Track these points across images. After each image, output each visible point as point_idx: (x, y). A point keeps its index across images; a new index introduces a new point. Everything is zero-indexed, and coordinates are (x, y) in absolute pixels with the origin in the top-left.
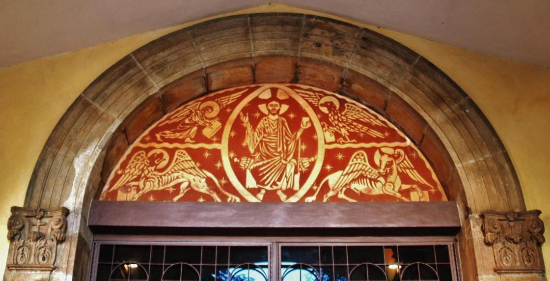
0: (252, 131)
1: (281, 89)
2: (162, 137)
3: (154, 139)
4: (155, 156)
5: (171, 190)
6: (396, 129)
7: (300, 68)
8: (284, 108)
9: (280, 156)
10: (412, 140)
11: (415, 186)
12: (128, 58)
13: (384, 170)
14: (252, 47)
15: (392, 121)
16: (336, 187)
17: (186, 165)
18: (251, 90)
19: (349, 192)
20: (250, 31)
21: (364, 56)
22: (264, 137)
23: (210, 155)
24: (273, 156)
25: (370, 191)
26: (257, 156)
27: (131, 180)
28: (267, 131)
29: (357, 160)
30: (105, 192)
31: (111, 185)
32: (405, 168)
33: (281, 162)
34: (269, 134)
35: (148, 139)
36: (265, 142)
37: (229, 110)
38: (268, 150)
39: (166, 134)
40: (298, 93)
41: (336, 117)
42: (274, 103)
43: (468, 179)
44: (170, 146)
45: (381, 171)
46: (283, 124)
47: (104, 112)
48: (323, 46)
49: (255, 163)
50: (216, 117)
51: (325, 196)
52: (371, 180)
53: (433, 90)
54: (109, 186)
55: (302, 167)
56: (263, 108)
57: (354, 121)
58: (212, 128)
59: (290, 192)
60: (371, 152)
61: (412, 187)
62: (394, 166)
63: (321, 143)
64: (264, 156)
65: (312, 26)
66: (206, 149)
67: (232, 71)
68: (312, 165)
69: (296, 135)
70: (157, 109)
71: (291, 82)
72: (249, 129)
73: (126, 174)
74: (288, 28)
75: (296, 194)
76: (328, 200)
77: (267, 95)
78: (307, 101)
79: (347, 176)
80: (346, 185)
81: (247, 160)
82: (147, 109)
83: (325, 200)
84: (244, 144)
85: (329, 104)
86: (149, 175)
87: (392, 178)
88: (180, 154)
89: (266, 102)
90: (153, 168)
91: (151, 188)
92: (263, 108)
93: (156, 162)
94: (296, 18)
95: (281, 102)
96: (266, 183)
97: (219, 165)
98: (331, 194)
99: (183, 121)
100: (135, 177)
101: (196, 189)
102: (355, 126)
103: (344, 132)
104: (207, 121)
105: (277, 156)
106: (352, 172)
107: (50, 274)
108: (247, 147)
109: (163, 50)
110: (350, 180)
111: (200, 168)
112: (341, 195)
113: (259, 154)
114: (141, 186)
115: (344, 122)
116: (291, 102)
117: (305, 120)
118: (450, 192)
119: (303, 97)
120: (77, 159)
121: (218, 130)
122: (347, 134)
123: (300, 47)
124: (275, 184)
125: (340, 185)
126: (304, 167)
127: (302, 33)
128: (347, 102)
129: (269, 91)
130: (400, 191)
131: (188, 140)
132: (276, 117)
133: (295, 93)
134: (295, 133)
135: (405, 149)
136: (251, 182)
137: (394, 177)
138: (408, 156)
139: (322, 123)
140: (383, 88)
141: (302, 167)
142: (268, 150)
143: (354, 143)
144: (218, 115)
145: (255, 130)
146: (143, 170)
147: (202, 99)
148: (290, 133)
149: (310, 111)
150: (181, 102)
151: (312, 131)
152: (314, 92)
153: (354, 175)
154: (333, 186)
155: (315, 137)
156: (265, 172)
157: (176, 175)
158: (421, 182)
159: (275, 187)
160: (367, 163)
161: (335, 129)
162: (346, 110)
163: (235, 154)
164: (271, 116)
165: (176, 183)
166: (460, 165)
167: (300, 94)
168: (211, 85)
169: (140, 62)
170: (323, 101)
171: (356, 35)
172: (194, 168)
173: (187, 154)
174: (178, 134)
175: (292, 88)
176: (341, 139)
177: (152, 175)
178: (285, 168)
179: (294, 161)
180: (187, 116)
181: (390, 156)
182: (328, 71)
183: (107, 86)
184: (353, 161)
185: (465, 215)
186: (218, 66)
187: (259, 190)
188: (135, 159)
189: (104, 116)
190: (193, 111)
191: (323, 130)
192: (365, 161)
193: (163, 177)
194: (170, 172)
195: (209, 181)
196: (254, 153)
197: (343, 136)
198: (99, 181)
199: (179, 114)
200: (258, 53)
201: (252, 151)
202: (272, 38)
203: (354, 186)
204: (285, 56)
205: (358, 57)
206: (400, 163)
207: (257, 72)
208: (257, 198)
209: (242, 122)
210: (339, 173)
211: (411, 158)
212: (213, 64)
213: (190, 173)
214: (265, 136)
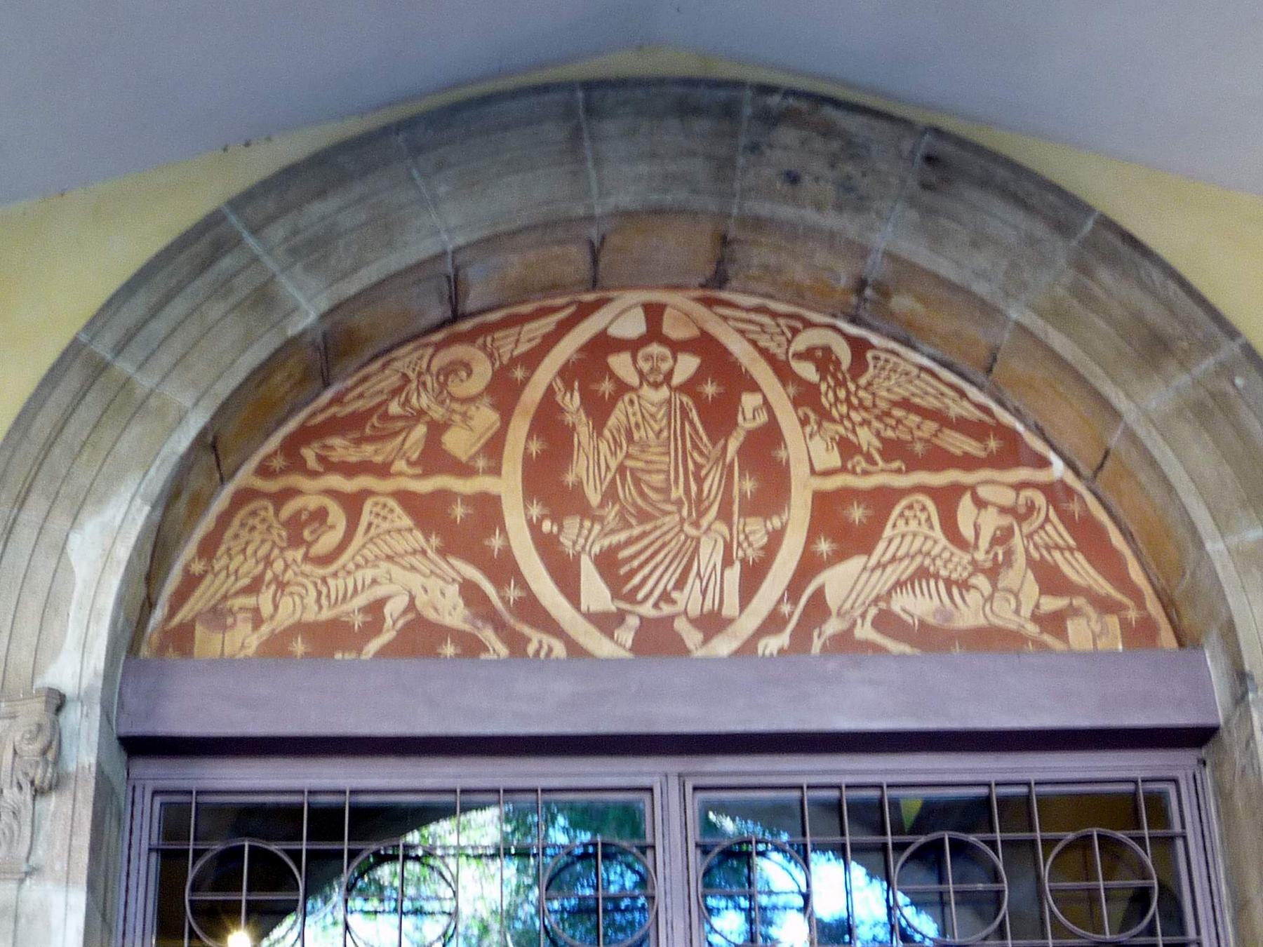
0: (591, 437)
1: (674, 307)
2: (321, 459)
3: (297, 465)
4: (304, 517)
5: (358, 620)
6: (1020, 427)
7: (735, 247)
8: (687, 365)
9: (680, 511)
10: (1070, 464)
11: (1079, 601)
12: (213, 220)
13: (987, 552)
14: (594, 185)
15: (1009, 404)
16: (847, 606)
17: (400, 544)
18: (585, 311)
19: (887, 622)
20: (586, 135)
21: (928, 212)
22: (628, 456)
23: (470, 512)
24: (657, 514)
25: (948, 617)
26: (611, 513)
27: (233, 591)
28: (636, 436)
29: (907, 523)
30: (154, 629)
31: (173, 612)
32: (1048, 548)
33: (682, 530)
34: (644, 447)
35: (278, 463)
36: (633, 471)
37: (519, 373)
38: (642, 494)
39: (332, 448)
40: (725, 318)
41: (842, 394)
42: (655, 349)
43: (1243, 587)
44: (349, 485)
45: (980, 556)
46: (685, 413)
47: (152, 391)
48: (807, 180)
49: (606, 535)
50: (480, 395)
51: (816, 633)
52: (949, 583)
53: (1139, 317)
54: (166, 610)
55: (745, 545)
56: (620, 363)
57: (895, 404)
58: (471, 429)
59: (712, 623)
60: (946, 499)
61: (1071, 604)
62: (1017, 542)
63: (799, 472)
64: (631, 514)
65: (771, 120)
66: (456, 494)
67: (531, 256)
68: (776, 538)
69: (725, 449)
70: (305, 379)
71: (703, 286)
72: (584, 432)
73: (216, 575)
74: (702, 125)
75: (730, 629)
76: (824, 645)
77: (632, 326)
78: (754, 343)
79: (878, 572)
80: (876, 600)
81: (581, 526)
82: (278, 378)
83: (817, 645)
84: (570, 479)
85: (819, 354)
86: (289, 575)
87: (1009, 578)
88: (378, 509)
89: (633, 346)
90: (299, 554)
91: (297, 616)
92: (620, 363)
93: (306, 534)
94: (722, 94)
95: (677, 347)
96: (640, 596)
97: (496, 542)
98: (833, 626)
99: (383, 408)
100: (245, 581)
101: (431, 615)
102: (899, 421)
103: (865, 437)
104: (456, 406)
105: (669, 513)
106: (893, 559)
107: (19, 889)
108: (579, 486)
109: (321, 194)
110: (889, 584)
111: (443, 552)
112: (865, 632)
113: (617, 507)
114: (266, 609)
115: (866, 409)
116: (705, 345)
117: (749, 401)
118: (1186, 622)
119: (742, 332)
120: (78, 536)
121: (489, 434)
122: (877, 443)
123: (737, 185)
124: (666, 597)
125: (860, 601)
126: (750, 545)
127: (743, 141)
128: (872, 347)
129: (639, 315)
130: (1036, 618)
131: (400, 465)
132: (664, 392)
133: (717, 318)
134: (722, 442)
135: (1048, 489)
136: (595, 593)
137: (1019, 576)
138: (1056, 509)
139: (801, 412)
140: (987, 311)
141: (745, 545)
142: (642, 494)
143: (899, 471)
144: (490, 389)
145: (600, 434)
146: (268, 562)
147: (438, 337)
148: (705, 438)
149: (762, 372)
150: (376, 350)
151: (770, 435)
152: (774, 315)
153: (898, 572)
154: (839, 603)
155: (782, 454)
156: (636, 563)
157: (369, 573)
158: (1095, 587)
159: (667, 609)
160: (938, 533)
161: (841, 430)
162: (871, 371)
163: (544, 506)
164: (646, 391)
165: (372, 598)
166: (1220, 546)
167: (731, 323)
168: (466, 294)
169: (255, 231)
170: (800, 344)
171: (906, 145)
172: (424, 552)
173: (398, 510)
174: (368, 450)
175: (709, 303)
176: (858, 458)
177: (295, 574)
178: (696, 549)
179: (721, 527)
180: (396, 392)
181: (1003, 510)
182: (821, 257)
183: (155, 311)
184: (894, 526)
185: (1233, 695)
186: (489, 244)
187: (620, 617)
188: (243, 525)
189: (153, 402)
190: (412, 376)
191: (804, 433)
192: (931, 527)
193: (331, 582)
194: (351, 566)
195: (470, 592)
196: (602, 505)
197: (865, 448)
198: (142, 599)
199: (367, 385)
200: (612, 202)
201: (594, 498)
202: (654, 155)
203: (903, 603)
204: (695, 213)
205: (913, 215)
206: (1036, 531)
207: (604, 260)
208: (616, 642)
209: (562, 410)
210: (854, 564)
211: (1065, 518)
212: (475, 236)
213: (413, 568)
214: (634, 450)
